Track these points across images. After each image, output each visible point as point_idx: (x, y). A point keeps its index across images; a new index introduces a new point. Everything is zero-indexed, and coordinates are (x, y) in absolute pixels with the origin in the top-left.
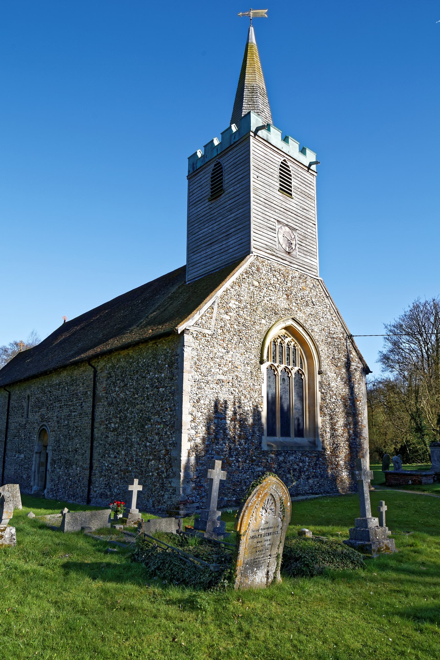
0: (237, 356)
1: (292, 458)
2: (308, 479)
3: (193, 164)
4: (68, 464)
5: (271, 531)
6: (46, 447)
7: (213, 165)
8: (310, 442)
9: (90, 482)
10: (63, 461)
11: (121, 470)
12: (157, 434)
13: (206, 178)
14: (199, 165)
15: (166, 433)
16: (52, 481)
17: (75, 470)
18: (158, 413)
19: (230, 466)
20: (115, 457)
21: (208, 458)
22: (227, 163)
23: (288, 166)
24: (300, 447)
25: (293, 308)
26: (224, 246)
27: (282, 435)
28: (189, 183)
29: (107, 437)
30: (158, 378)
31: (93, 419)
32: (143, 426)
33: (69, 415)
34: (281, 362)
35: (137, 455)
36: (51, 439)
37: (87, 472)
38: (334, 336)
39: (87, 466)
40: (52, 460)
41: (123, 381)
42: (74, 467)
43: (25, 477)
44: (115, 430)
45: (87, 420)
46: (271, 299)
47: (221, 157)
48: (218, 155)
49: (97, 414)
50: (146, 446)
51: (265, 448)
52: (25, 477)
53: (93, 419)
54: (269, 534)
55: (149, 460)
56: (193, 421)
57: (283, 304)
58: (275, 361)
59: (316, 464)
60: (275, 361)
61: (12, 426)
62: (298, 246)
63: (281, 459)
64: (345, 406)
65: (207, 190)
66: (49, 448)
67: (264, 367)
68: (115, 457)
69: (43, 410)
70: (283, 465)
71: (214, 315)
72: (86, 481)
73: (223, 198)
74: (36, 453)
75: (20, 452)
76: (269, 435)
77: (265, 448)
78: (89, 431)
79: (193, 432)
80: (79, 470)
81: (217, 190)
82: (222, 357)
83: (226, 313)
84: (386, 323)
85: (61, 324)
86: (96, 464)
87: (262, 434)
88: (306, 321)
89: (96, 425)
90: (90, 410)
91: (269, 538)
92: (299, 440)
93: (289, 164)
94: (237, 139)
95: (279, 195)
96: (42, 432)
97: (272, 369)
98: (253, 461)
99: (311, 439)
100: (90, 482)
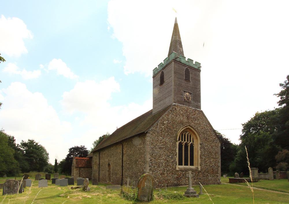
0: (167, 140)
2: (194, 180)
4: (116, 174)
5: (148, 188)
6: (110, 169)
7: (161, 73)
8: (196, 168)
9: (122, 179)
10: (115, 173)
12: (140, 165)
16: (112, 179)
17: (118, 176)
19: (164, 175)
20: (129, 172)
21: (156, 172)
22: (165, 72)
23: (188, 70)
24: (191, 170)
25: (190, 122)
26: (164, 102)
27: (185, 165)
28: (153, 79)
29: (127, 166)
31: (122, 161)
32: (136, 162)
33: (116, 159)
35: (135, 171)
36: (111, 166)
37: (121, 177)
38: (207, 131)
39: (121, 175)
40: (112, 173)
41: (130, 148)
43: (105, 178)
44: (129, 164)
45: (121, 161)
46: (180, 119)
47: (164, 69)
48: (162, 69)
49: (124, 159)
50: (137, 168)
51: (177, 169)
52: (105, 178)
53: (122, 161)
54: (148, 189)
59: (198, 175)
60: (182, 140)
61: (101, 163)
62: (192, 99)
63: (184, 173)
64: (92, 160)
65: (159, 82)
66: (111, 169)
67: (178, 143)
71: (158, 126)
72: (121, 179)
73: (164, 84)
75: (103, 171)
76: (179, 165)
77: (177, 169)
78: (121, 164)
79: (151, 164)
80: (119, 176)
81: (162, 81)
82: (161, 140)
83: (163, 125)
84: (243, 124)
85: (115, 129)
87: (177, 165)
89: (123, 162)
90: (121, 158)
91: (148, 190)
92: (192, 167)
93: (189, 69)
94: (168, 63)
96: (109, 165)
98: (173, 173)
99: (197, 166)
100: (122, 179)
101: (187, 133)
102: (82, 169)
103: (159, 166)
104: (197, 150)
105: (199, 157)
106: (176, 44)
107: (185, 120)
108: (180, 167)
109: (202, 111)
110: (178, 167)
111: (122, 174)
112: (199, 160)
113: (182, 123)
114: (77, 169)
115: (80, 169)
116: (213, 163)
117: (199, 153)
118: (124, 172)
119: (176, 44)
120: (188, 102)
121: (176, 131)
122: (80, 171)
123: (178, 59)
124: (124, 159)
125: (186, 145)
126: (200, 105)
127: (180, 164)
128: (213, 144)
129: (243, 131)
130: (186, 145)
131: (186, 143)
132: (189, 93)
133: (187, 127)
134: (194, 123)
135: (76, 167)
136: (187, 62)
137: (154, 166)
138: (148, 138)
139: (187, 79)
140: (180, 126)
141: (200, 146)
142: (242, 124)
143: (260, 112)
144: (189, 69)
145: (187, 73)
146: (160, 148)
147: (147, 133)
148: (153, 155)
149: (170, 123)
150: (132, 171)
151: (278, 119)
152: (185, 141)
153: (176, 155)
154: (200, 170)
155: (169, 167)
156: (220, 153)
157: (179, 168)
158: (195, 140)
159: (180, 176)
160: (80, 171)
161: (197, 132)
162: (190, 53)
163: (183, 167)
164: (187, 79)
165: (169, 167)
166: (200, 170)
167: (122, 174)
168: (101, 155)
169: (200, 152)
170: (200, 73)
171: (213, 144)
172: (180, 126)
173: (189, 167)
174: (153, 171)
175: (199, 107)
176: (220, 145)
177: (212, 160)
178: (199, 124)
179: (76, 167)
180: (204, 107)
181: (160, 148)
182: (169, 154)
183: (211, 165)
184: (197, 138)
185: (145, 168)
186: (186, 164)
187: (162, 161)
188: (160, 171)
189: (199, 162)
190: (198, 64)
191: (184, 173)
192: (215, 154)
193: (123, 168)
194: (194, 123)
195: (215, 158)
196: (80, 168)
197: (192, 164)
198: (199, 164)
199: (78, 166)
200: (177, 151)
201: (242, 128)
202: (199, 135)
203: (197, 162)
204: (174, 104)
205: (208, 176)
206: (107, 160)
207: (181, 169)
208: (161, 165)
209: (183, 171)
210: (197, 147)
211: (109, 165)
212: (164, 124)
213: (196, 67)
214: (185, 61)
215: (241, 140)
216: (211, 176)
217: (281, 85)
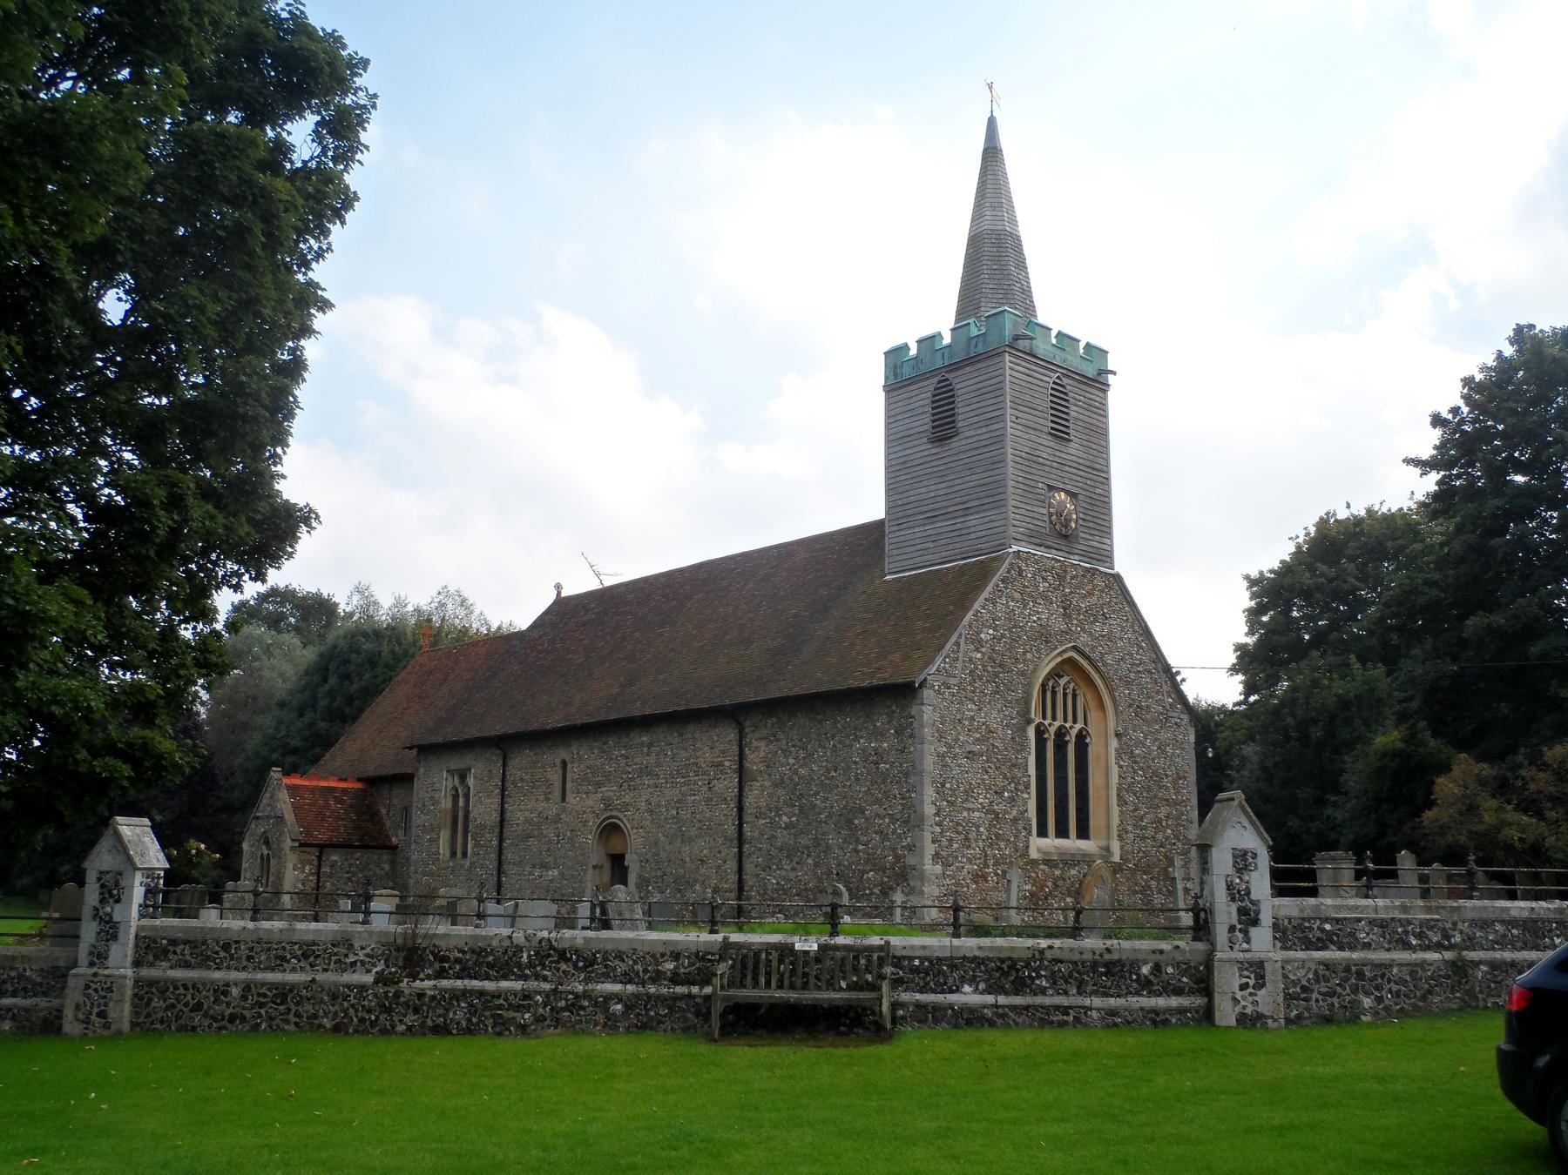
0: (993, 717)
1: (1073, 872)
3: (895, 367)
7: (936, 380)
11: (806, 890)
13: (922, 397)
14: (907, 372)
15: (894, 832)
18: (878, 801)
20: (793, 869)
22: (963, 384)
27: (1058, 836)
30: (875, 750)
31: (741, 809)
34: (1054, 718)
42: (698, 887)
44: (789, 826)
50: (857, 851)
51: (1034, 854)
53: (741, 809)
55: (864, 872)
56: (937, 814)
57: (1058, 624)
58: (1044, 717)
63: (1058, 872)
65: (925, 423)
68: (793, 869)
69: (609, 790)
70: (1060, 883)
73: (955, 444)
74: (595, 867)
75: (544, 866)
77: (1034, 854)
79: (938, 829)
81: (944, 427)
82: (972, 718)
83: (977, 650)
86: (750, 881)
88: (1093, 648)
89: (747, 818)
92: (1083, 845)
93: (1066, 381)
95: (1047, 441)
97: (1040, 732)
99: (1103, 843)
101: (1062, 681)
102: (334, 858)
103: (967, 839)
104: (1103, 762)
105: (1114, 793)
106: (993, 261)
107: (1058, 624)
108: (1042, 842)
109: (1118, 578)
110: (1040, 846)
111: (741, 882)
112: (1115, 810)
113: (1045, 637)
114: (306, 857)
115: (319, 858)
116: (1168, 826)
117: (1115, 780)
118: (749, 867)
119: (993, 261)
120: (1066, 537)
121: (1023, 673)
122: (319, 866)
123: (1022, 344)
124: (753, 799)
125: (1061, 734)
126: (1111, 546)
127: (1042, 832)
128: (1165, 735)
129: (1253, 615)
130: (1061, 734)
131: (1060, 728)
132: (1068, 493)
133: (1066, 656)
134: (1091, 634)
135: (301, 845)
136: (1057, 352)
137: (951, 840)
138: (929, 711)
139: (1060, 434)
140: (1038, 651)
141: (1114, 743)
142: (1247, 577)
143: (1342, 514)
144: (1066, 381)
145: (1059, 398)
146: (970, 755)
147: (922, 685)
148: (943, 785)
149: (1003, 636)
150: (817, 864)
151: (1434, 592)
152: (1054, 718)
153: (1027, 787)
154: (1117, 858)
155: (1002, 845)
156: (1192, 777)
157: (1039, 850)
158: (1094, 715)
159: (1042, 887)
160: (319, 866)
161: (1102, 677)
162: (1062, 302)
163: (1051, 843)
164: (1060, 434)
165: (1002, 845)
166: (1117, 858)
167: (741, 882)
168: (511, 770)
169: (1115, 770)
170: (1105, 398)
171: (1165, 735)
172: (1038, 651)
173: (1072, 844)
174: (946, 865)
175: (1106, 557)
176: (1192, 739)
177: (1163, 812)
178: (1110, 637)
179: (301, 845)
180: (1126, 562)
181: (970, 755)
182: (1000, 782)
183: (1160, 836)
184: (1102, 706)
185: (911, 848)
186: (1062, 832)
187: (977, 814)
188: (970, 861)
189: (1115, 821)
190: (1095, 353)
191: (1058, 872)
192: (1175, 782)
193: (746, 847)
194: (1091, 634)
195: (1176, 803)
196: (322, 847)
197: (1083, 833)
198: (1115, 833)
199: (308, 832)
200: (1032, 770)
201: (1244, 600)
202: (1111, 692)
203: (1103, 822)
204: (1015, 548)
205: (1150, 889)
206: (593, 802)
207: (1045, 853)
208: (972, 836)
209: (1056, 866)
210: (1102, 749)
211: (610, 830)
212: (979, 644)
213: (1090, 371)
214: (1050, 348)
215: (1240, 677)
216: (1160, 892)
217: (1437, 421)
